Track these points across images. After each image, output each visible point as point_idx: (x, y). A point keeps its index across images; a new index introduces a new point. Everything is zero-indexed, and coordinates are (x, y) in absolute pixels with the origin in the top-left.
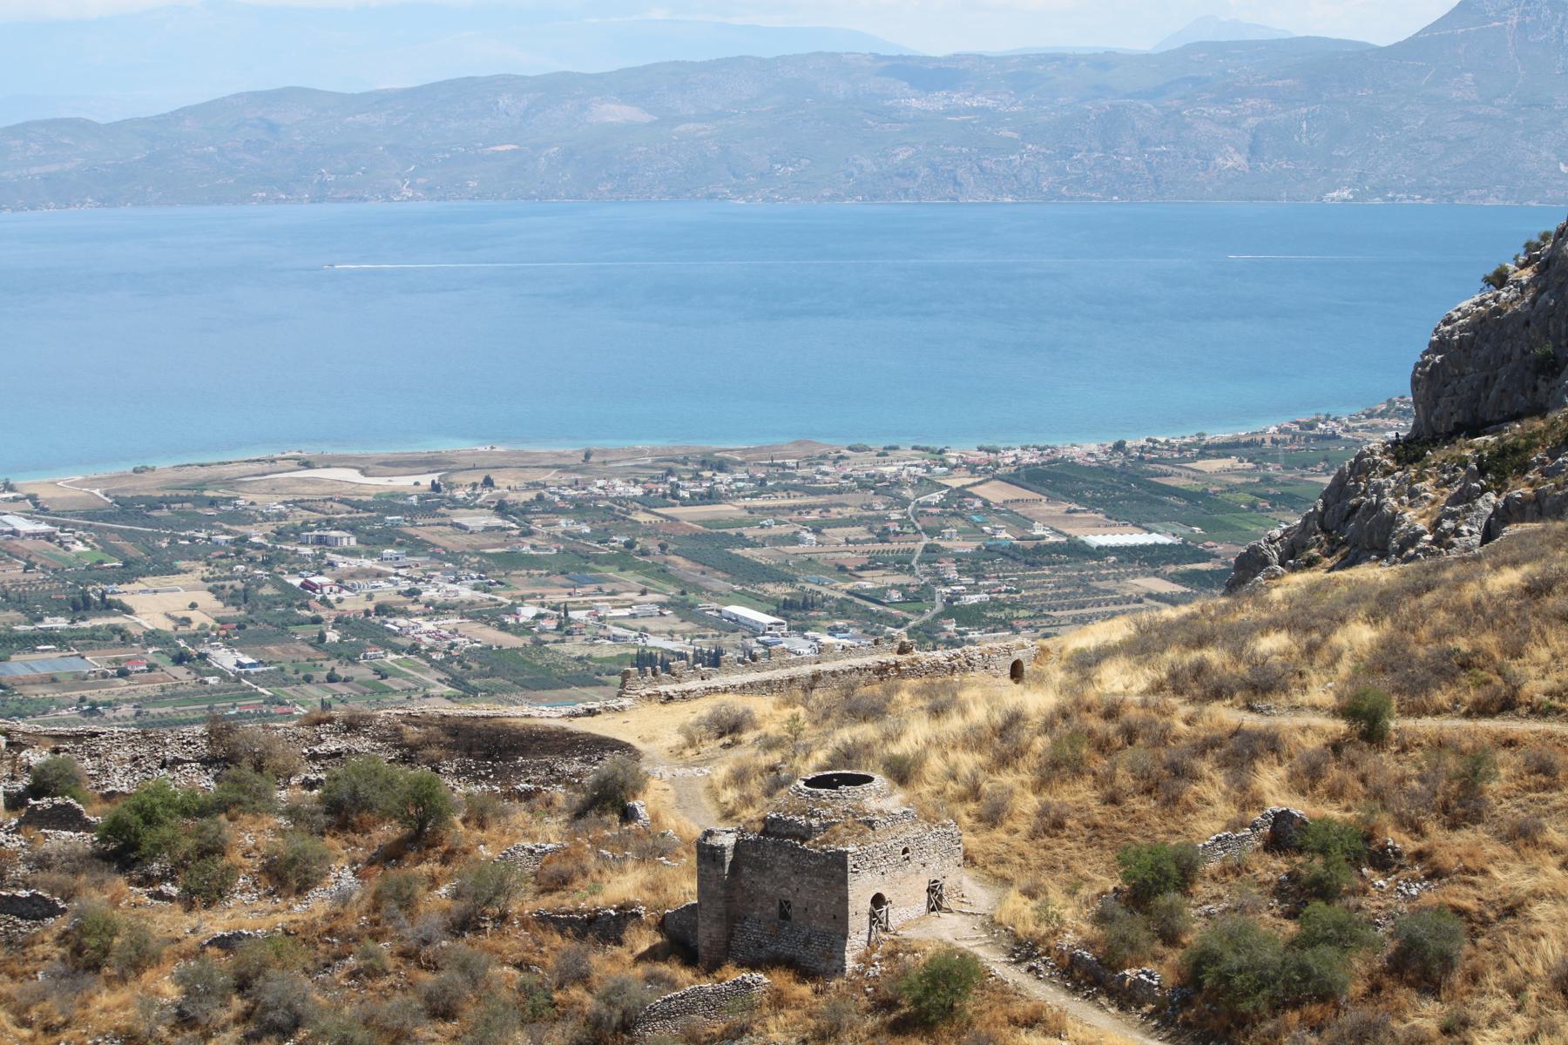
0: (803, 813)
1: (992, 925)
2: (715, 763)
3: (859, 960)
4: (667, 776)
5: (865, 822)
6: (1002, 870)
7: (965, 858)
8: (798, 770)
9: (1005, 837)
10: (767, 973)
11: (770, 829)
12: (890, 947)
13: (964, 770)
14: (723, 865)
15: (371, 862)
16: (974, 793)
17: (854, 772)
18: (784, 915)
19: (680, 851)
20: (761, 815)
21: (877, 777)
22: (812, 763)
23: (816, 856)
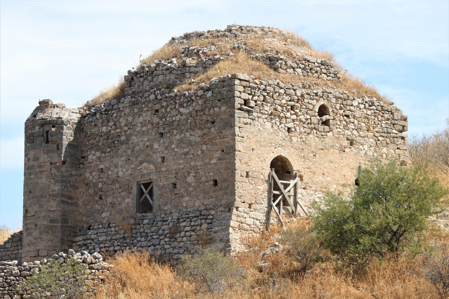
18: (145, 206)
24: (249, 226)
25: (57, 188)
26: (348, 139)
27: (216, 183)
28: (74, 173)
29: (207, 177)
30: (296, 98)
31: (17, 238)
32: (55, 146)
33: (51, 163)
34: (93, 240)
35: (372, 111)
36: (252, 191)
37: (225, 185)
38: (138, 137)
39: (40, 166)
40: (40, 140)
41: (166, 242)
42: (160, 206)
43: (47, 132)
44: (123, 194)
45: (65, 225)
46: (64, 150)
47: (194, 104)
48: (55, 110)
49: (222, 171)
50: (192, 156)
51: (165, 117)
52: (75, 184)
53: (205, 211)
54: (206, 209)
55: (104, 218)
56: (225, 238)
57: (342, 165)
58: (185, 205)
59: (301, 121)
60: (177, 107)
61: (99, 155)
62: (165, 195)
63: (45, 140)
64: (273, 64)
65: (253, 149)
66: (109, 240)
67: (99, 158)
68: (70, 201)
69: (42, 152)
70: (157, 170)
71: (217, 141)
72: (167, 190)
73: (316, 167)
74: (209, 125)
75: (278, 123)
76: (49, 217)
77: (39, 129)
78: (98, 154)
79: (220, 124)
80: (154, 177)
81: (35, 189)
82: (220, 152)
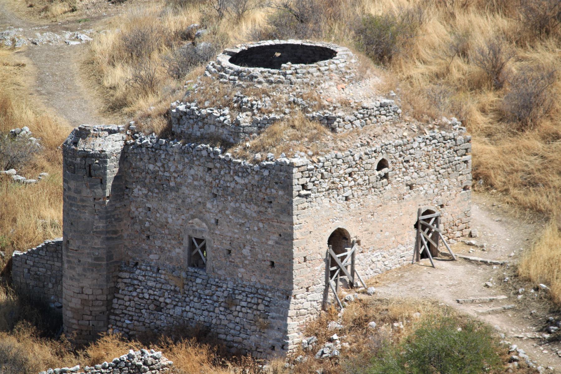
0: (228, 104)
1: (514, 280)
2: (99, 26)
3: (309, 331)
4: (23, 43)
5: (321, 120)
6: (532, 197)
7: (476, 178)
8: (224, 39)
9: (538, 145)
10: (167, 349)
11: (176, 129)
12: (355, 312)
13: (479, 42)
14: (103, 182)
15: (384, 65)
16: (494, 77)
17: (307, 43)
19: (40, 160)
20: (163, 106)
21: (340, 50)
22: (246, 28)
23: (245, 171)
24: (306, 310)
25: (101, 225)
26: (407, 185)
27: (273, 264)
28: (118, 205)
29: (263, 255)
30: (354, 163)
31: (53, 249)
32: (99, 181)
33: (95, 199)
34: (140, 281)
35: (434, 145)
36: (310, 275)
37: (283, 270)
38: (189, 189)
39: (82, 201)
40: (81, 173)
41: (221, 311)
42: (213, 268)
43: (90, 166)
44: (173, 242)
45: (111, 261)
46: (109, 185)
47: (250, 177)
48: (97, 141)
49: (280, 255)
50: (247, 229)
51: (218, 179)
52: (119, 216)
53: (262, 291)
54: (263, 289)
55: (152, 260)
56: (283, 328)
57: (401, 214)
58: (240, 276)
59: (359, 184)
60: (232, 173)
61: (146, 192)
62: (219, 259)
63: (88, 173)
64: (331, 124)
65: (310, 232)
66: (158, 288)
67: (146, 196)
68: (114, 236)
69: (84, 186)
70: (210, 230)
71: (275, 224)
72: (221, 254)
73: (373, 227)
74: (266, 204)
75: (336, 196)
76: (93, 255)
77: (81, 160)
78: (145, 191)
79: (277, 208)
80: (206, 236)
81: (78, 223)
82: (278, 236)
